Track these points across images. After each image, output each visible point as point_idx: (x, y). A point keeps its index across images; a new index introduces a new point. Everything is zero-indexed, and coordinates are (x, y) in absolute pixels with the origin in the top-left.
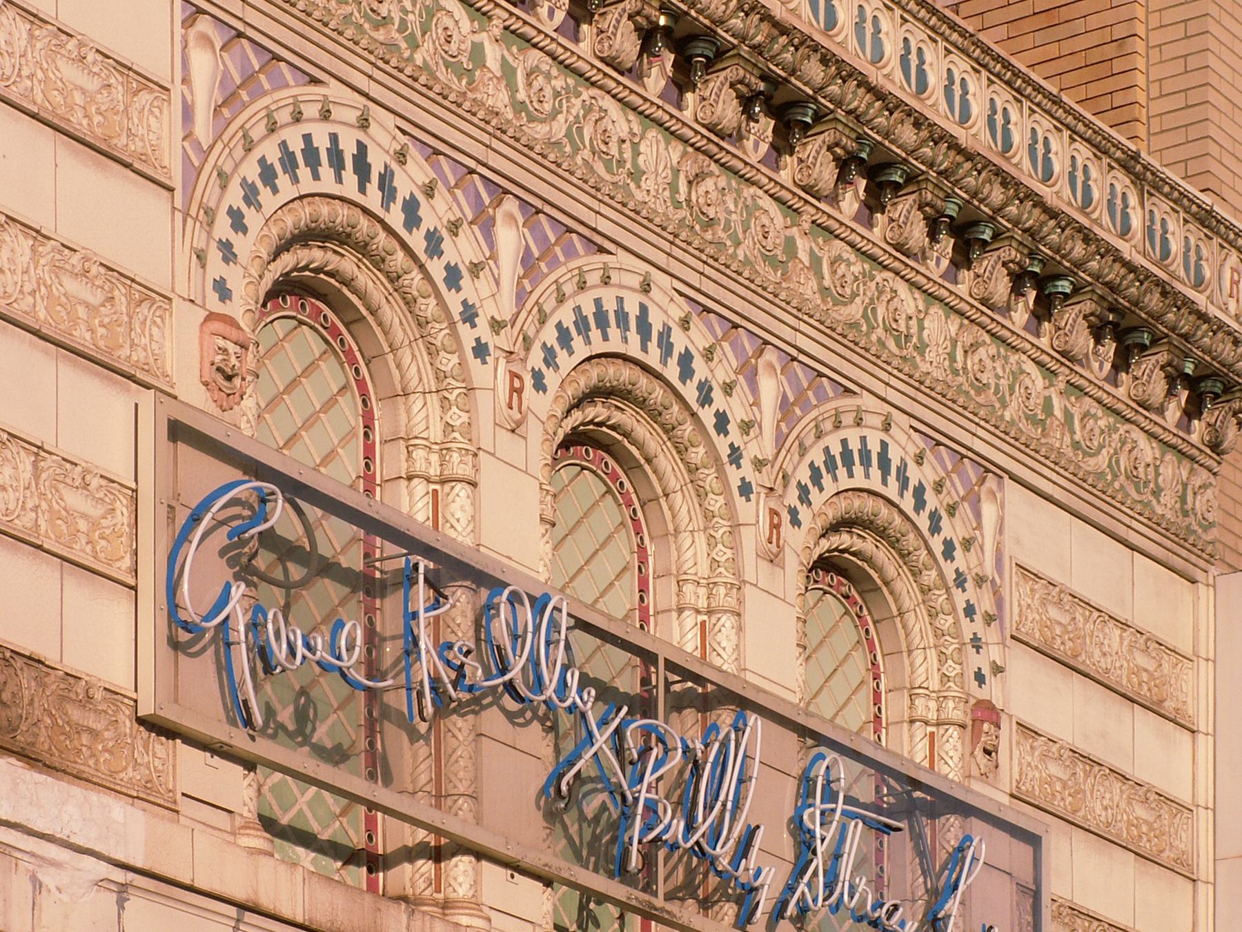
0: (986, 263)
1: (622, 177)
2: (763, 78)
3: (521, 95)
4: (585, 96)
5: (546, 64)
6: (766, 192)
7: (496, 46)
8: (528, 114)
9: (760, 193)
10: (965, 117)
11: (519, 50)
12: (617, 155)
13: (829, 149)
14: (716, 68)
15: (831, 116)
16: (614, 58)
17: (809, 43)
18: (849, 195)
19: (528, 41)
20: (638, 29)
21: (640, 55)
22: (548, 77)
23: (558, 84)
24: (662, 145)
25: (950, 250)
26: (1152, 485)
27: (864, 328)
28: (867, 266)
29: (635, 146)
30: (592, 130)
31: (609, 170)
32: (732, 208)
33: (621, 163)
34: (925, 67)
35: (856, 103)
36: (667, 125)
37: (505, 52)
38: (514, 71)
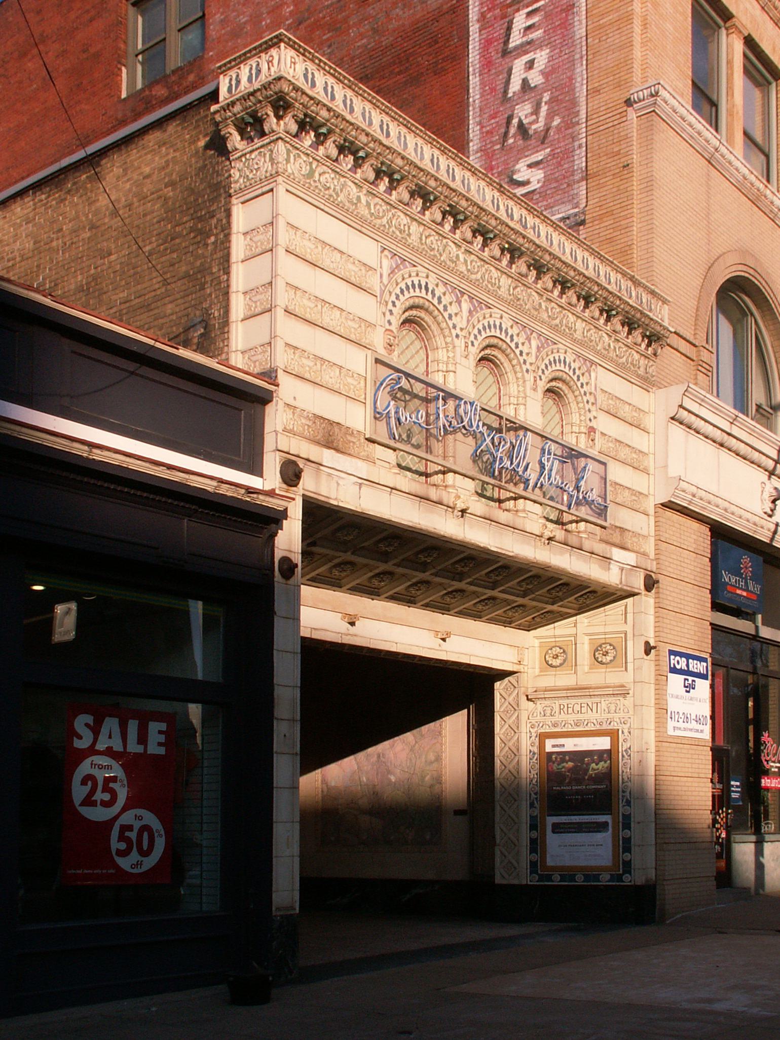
3: (373, 211)
5: (380, 202)
10: (422, 158)
22: (381, 206)
31: (400, 232)
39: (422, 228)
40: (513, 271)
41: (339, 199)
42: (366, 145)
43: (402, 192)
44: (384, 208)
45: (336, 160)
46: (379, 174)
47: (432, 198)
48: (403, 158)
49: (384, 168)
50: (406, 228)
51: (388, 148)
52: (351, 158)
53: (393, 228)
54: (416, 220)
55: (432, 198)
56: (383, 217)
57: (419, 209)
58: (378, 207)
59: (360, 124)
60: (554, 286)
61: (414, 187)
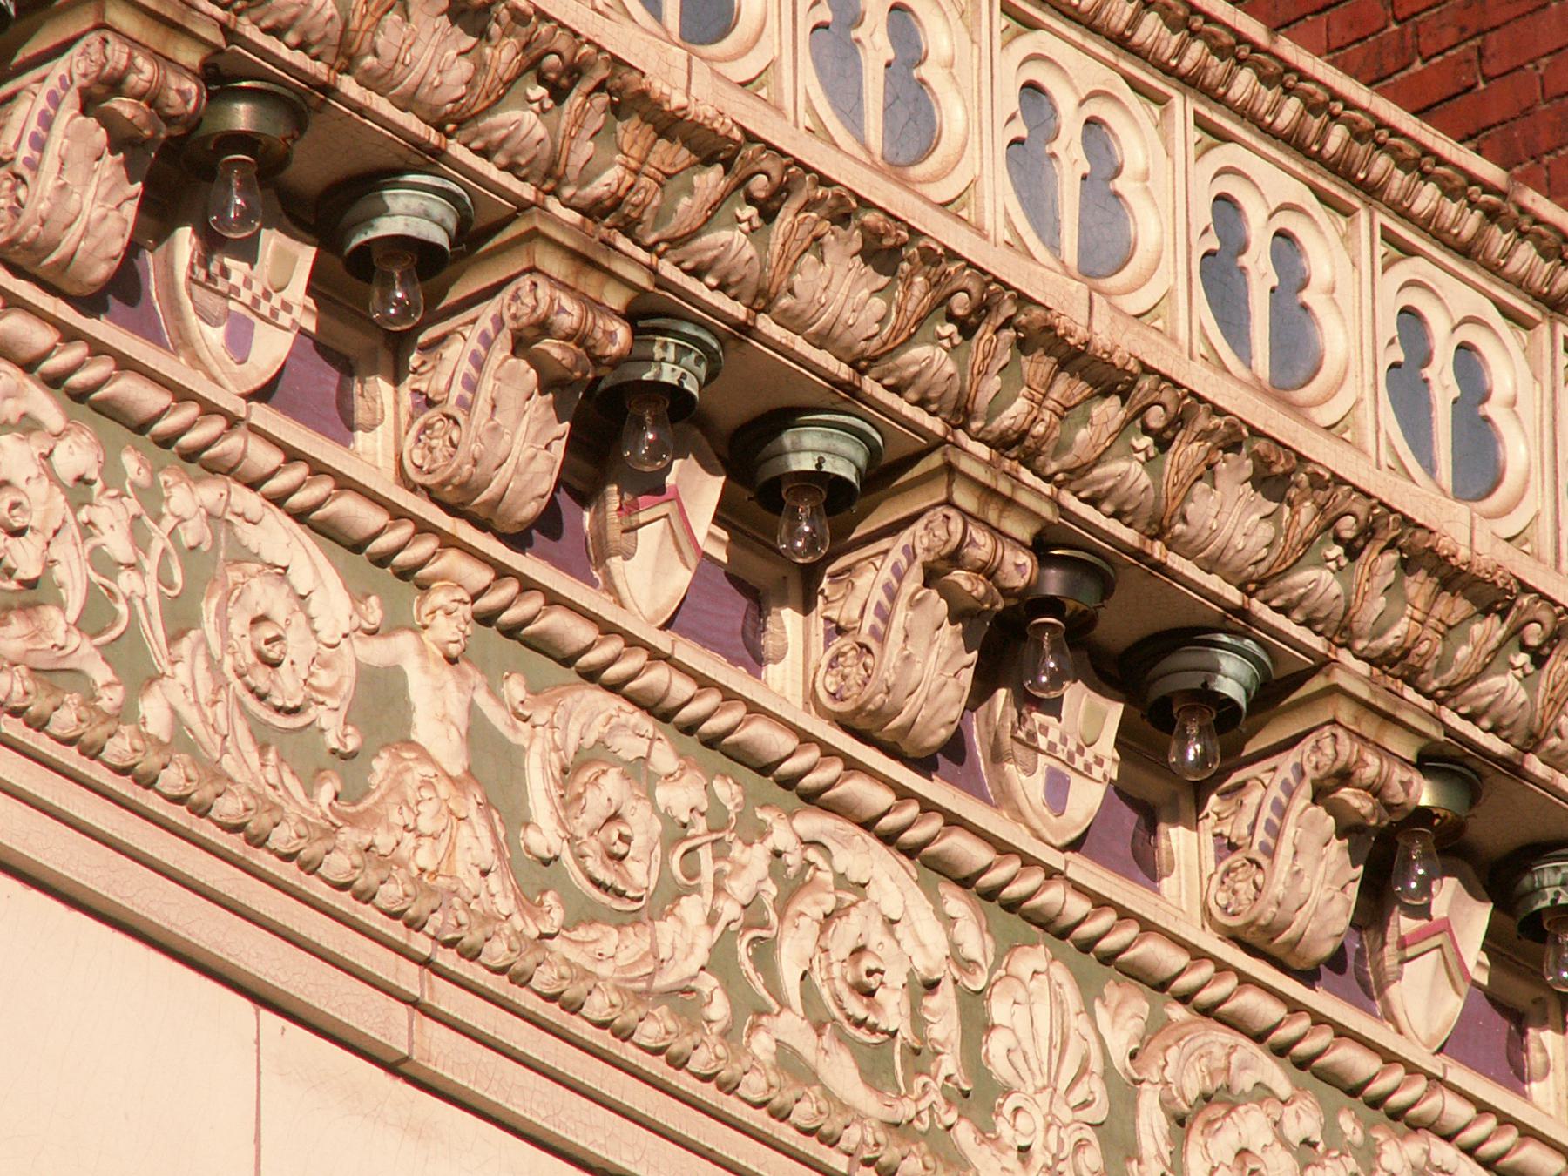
0: (870, 582)
1: (922, 1102)
2: (1430, 761)
3: (544, 836)
4: (781, 836)
5: (634, 734)
6: (1470, 1151)
7: (447, 674)
8: (568, 894)
9: (250, 501)
10: (1106, 253)
11: (534, 691)
12: (906, 1032)
13: (1320, 794)
14: (455, 295)
15: (1316, 684)
16: (1272, 930)
17: (1203, 422)
18: (650, 537)
19: (567, 661)
20: (1349, 829)
21: (980, 693)
22: (639, 772)
23: (681, 797)
24: (1071, 995)
25: (1106, 746)
26: (949, 1064)
27: (719, 1010)
28: (727, 791)
29: (974, 1007)
30: (809, 945)
31: (874, 1071)
32: (118, 545)
33: (919, 1055)
34: (1490, 409)
35: (1020, 407)
36: (1377, 1087)
37: (483, 699)
38: (512, 758)
39: (1122, 1019)
40: (782, 684)
41: (154, 711)
42: (454, 120)
43: (890, 627)
44: (681, 797)
45: (122, 290)
46: (609, 429)
47: (1232, 678)
48: (885, 251)
49: (670, 367)
50: (944, 1022)
51: (712, 147)
52: (285, 264)
53: (791, 1026)
54: (1055, 929)
55: (1232, 678)
56: (669, 896)
57: (1086, 799)
58: (610, 788)
59: (1198, 378)
60: (1378, 896)
61: (1019, 567)
